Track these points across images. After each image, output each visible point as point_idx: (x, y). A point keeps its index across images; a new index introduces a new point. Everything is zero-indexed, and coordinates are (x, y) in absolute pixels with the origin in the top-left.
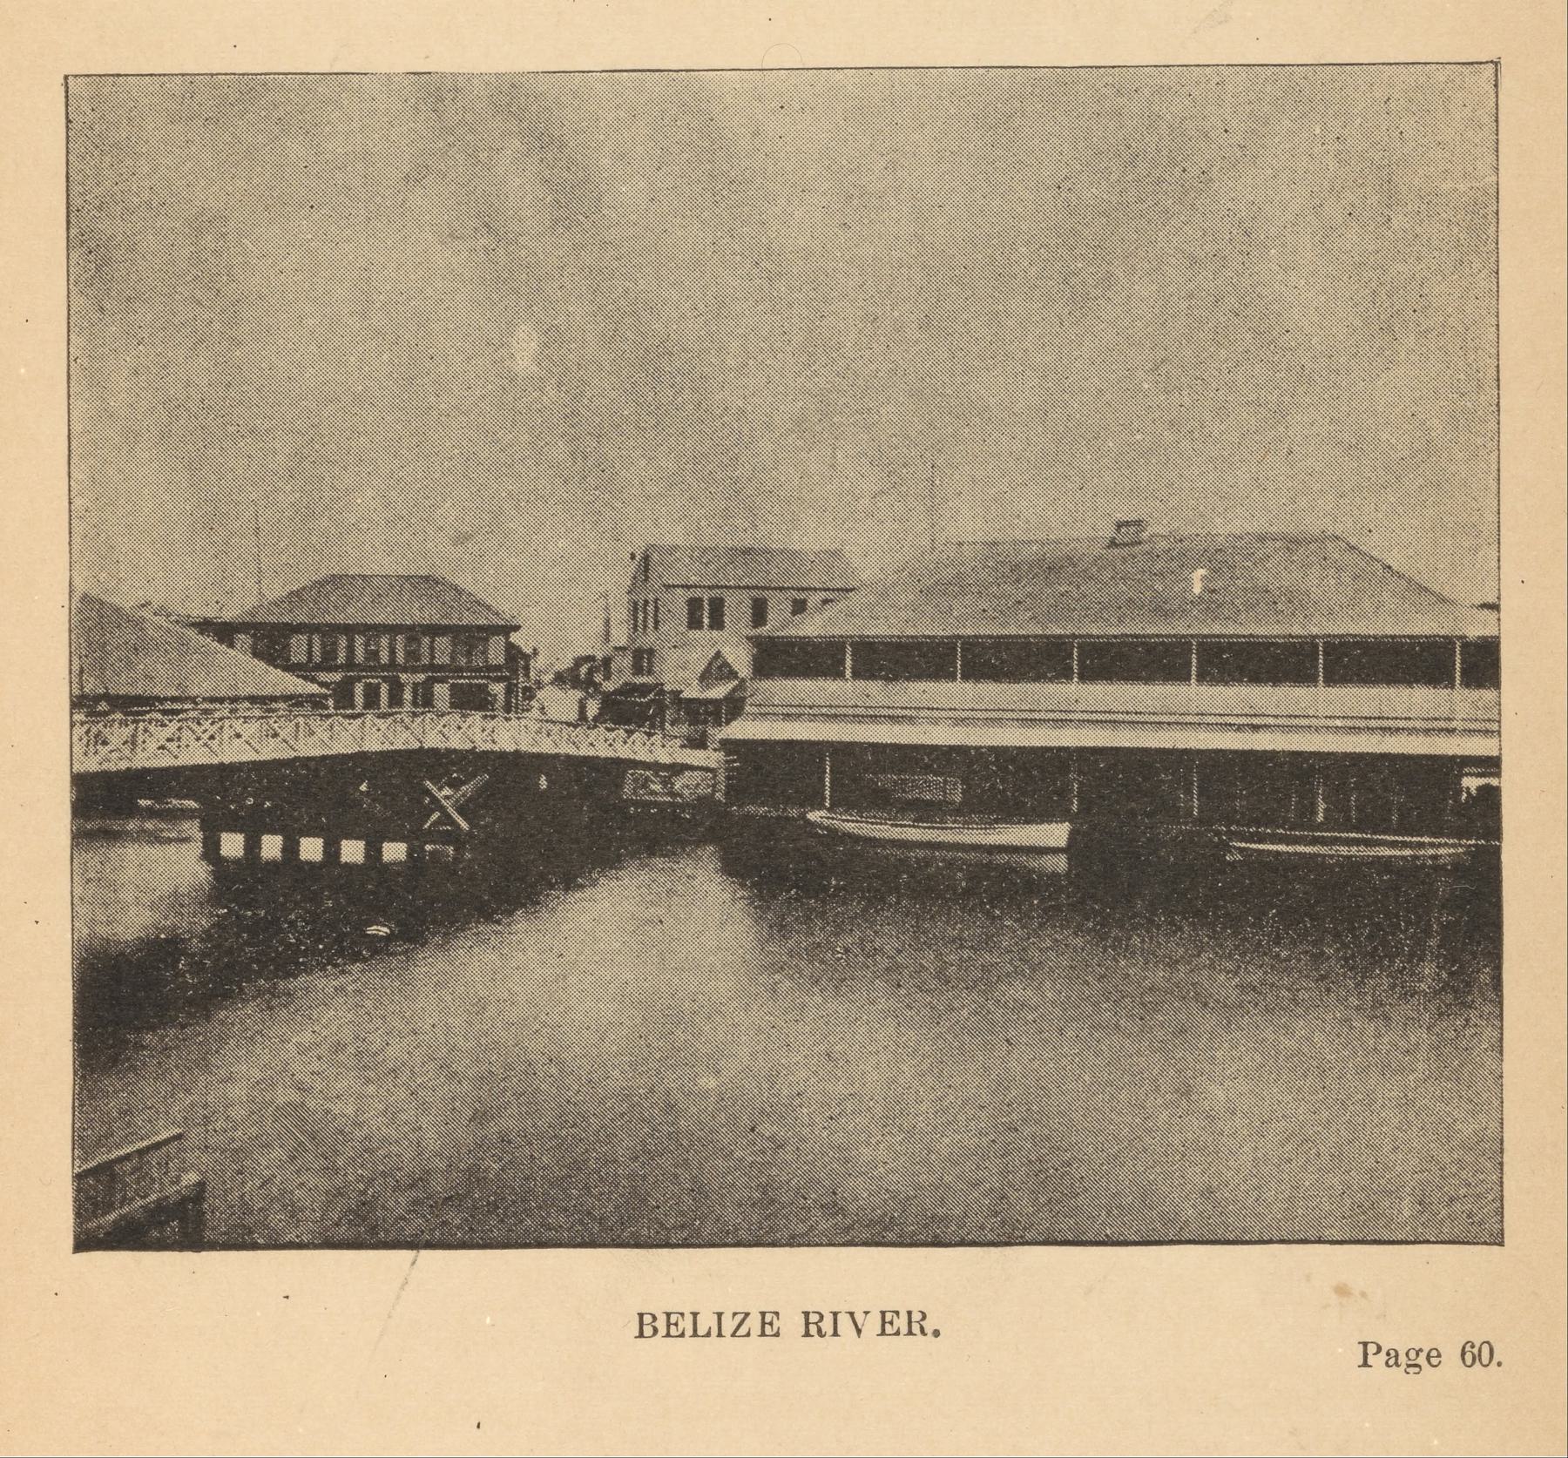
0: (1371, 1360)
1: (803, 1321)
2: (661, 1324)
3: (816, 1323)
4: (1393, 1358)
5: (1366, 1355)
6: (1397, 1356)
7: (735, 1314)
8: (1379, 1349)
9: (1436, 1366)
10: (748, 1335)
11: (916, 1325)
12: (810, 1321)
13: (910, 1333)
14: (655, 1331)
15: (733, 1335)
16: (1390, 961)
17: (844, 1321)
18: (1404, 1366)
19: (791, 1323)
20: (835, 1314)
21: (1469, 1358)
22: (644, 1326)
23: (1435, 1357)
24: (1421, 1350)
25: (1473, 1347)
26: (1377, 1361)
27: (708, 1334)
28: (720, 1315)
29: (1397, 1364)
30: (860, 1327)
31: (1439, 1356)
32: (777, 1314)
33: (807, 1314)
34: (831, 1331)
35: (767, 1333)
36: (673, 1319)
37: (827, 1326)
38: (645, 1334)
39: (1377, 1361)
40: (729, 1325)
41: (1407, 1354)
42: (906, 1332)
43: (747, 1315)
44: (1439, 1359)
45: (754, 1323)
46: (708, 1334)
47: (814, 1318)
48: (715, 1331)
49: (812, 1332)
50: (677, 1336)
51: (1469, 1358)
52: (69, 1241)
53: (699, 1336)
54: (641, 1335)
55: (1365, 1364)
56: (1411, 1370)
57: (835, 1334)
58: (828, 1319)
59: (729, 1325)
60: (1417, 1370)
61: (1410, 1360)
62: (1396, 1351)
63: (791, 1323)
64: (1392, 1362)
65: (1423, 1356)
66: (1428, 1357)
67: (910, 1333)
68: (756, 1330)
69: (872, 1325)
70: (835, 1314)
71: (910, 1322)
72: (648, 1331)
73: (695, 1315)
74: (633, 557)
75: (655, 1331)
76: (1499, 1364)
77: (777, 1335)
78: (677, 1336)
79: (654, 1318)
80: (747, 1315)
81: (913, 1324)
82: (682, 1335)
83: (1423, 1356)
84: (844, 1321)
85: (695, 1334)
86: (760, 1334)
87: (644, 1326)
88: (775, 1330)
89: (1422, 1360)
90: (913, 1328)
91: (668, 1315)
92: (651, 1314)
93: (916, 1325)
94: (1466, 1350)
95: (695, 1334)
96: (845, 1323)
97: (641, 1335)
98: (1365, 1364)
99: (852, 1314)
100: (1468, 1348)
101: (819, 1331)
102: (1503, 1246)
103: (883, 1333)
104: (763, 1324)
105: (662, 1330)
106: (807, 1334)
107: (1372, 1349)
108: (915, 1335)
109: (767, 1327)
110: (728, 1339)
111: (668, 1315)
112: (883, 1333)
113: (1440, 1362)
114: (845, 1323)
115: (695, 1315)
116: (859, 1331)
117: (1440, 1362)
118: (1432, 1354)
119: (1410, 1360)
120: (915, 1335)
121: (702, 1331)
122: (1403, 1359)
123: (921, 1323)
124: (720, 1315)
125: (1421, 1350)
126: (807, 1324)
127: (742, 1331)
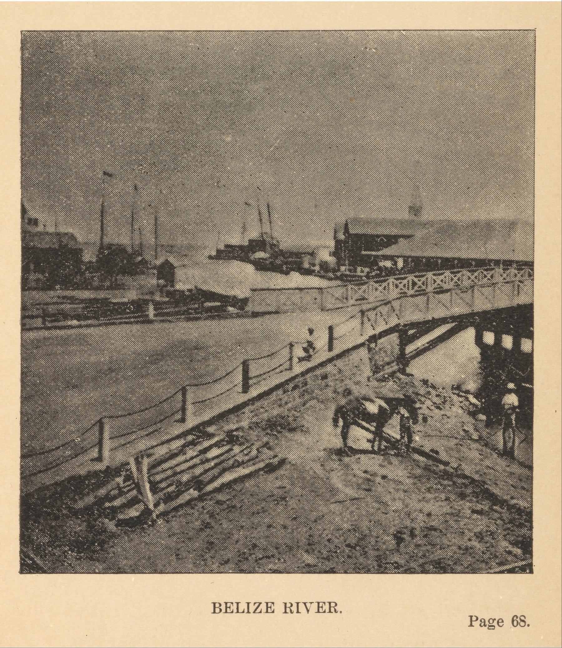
0: (474, 623)
1: (284, 607)
2: (223, 607)
3: (289, 607)
4: (483, 623)
5: (471, 621)
6: (485, 622)
7: (255, 603)
8: (477, 619)
9: (501, 627)
10: (261, 612)
11: (332, 608)
12: (331, 606)
13: (330, 612)
14: (221, 610)
15: (254, 612)
16: (29, 529)
17: (301, 606)
18: (487, 626)
19: (279, 608)
20: (298, 603)
21: (515, 623)
22: (216, 608)
23: (500, 622)
24: (495, 619)
25: (517, 618)
26: (476, 624)
27: (243, 612)
28: (248, 604)
29: (485, 625)
30: (308, 608)
31: (503, 622)
32: (273, 603)
33: (471, 617)
34: (295, 611)
35: (320, 611)
36: (228, 605)
37: (294, 608)
38: (216, 612)
39: (476, 624)
40: (252, 608)
41: (489, 621)
42: (328, 611)
43: (260, 603)
44: (502, 623)
45: (263, 607)
46: (243, 612)
47: (289, 605)
48: (246, 611)
49: (287, 612)
50: (270, 613)
51: (515, 623)
52: (18, 567)
53: (320, 612)
54: (214, 612)
55: (471, 625)
56: (489, 628)
57: (298, 612)
58: (295, 605)
59: (252, 608)
60: (493, 628)
61: (490, 623)
62: (484, 620)
63: (279, 608)
64: (482, 624)
65: (496, 622)
66: (498, 622)
67: (330, 612)
68: (264, 610)
69: (314, 607)
70: (298, 603)
71: (330, 607)
72: (217, 610)
73: (238, 603)
74: (422, 446)
75: (221, 610)
76: (528, 625)
77: (273, 612)
78: (270, 613)
79: (220, 605)
80: (260, 603)
81: (287, 608)
82: (325, 612)
83: (496, 622)
84: (301, 606)
85: (238, 612)
86: (284, 612)
87: (216, 608)
88: (231, 611)
89: (495, 624)
90: (216, 610)
91: (226, 603)
92: (334, 602)
93: (332, 608)
94: (514, 619)
95: (238, 612)
96: (302, 608)
97: (214, 612)
98: (471, 625)
99: (305, 604)
100: (515, 618)
101: (291, 610)
102: (21, 572)
103: (318, 612)
104: (267, 608)
105: (224, 610)
106: (286, 612)
107: (474, 619)
108: (332, 612)
109: (269, 609)
110: (252, 614)
111: (226, 603)
112: (318, 612)
113: (503, 624)
114: (302, 608)
115: (238, 603)
116: (308, 611)
117: (503, 624)
118: (500, 621)
119: (490, 623)
120: (332, 612)
121: (241, 610)
122: (487, 623)
123: (335, 607)
124: (248, 604)
125: (495, 619)
126: (286, 607)
127: (258, 610)
